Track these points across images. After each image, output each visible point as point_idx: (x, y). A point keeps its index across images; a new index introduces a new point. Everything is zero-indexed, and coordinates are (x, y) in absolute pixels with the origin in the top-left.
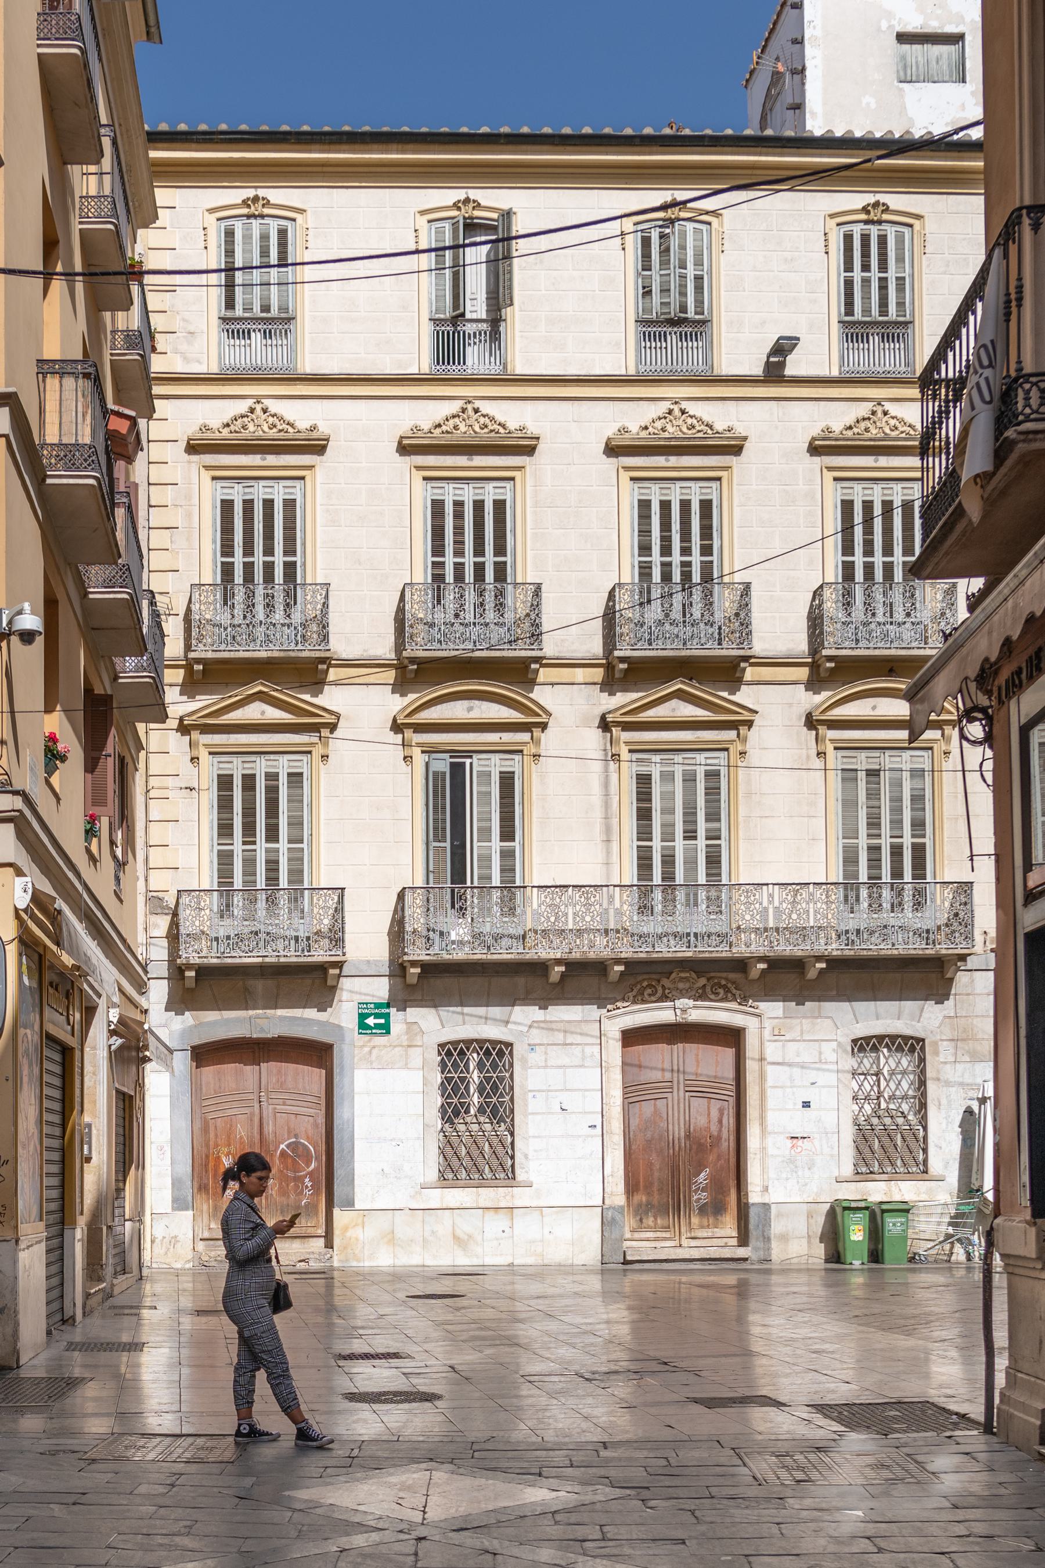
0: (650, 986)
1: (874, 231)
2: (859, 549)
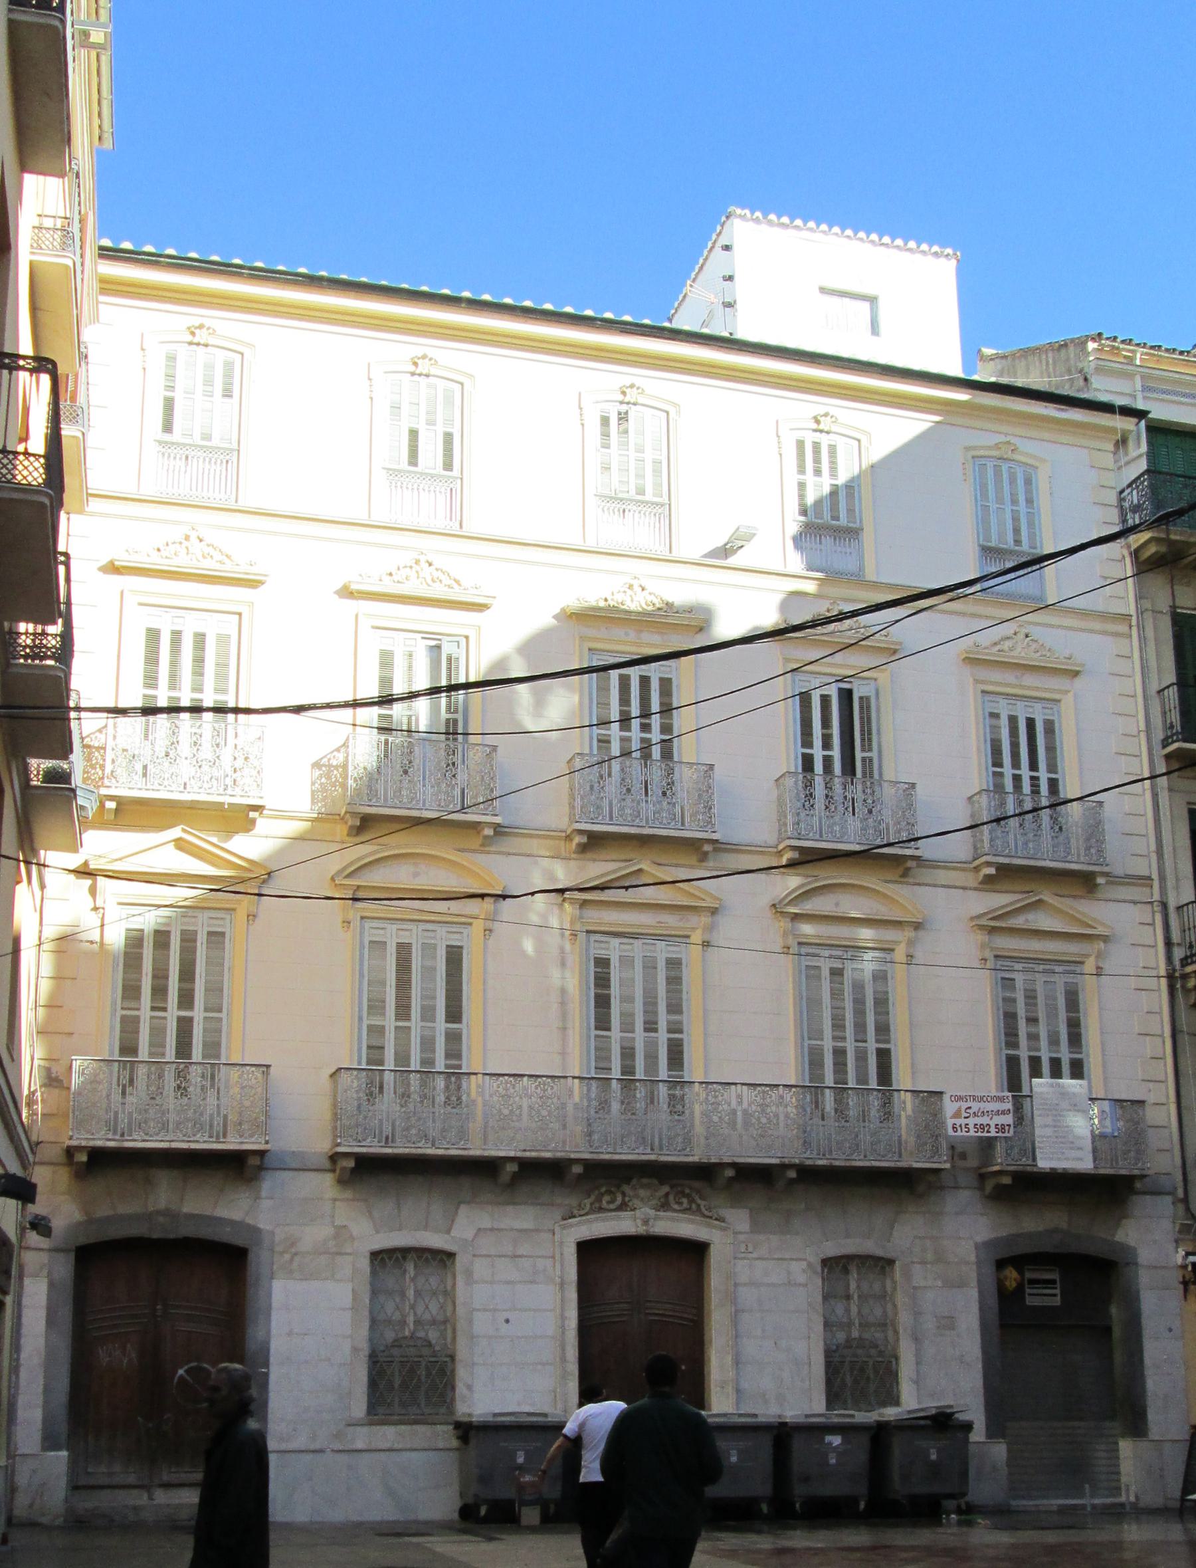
0: (609, 1192)
1: (825, 440)
2: (818, 742)
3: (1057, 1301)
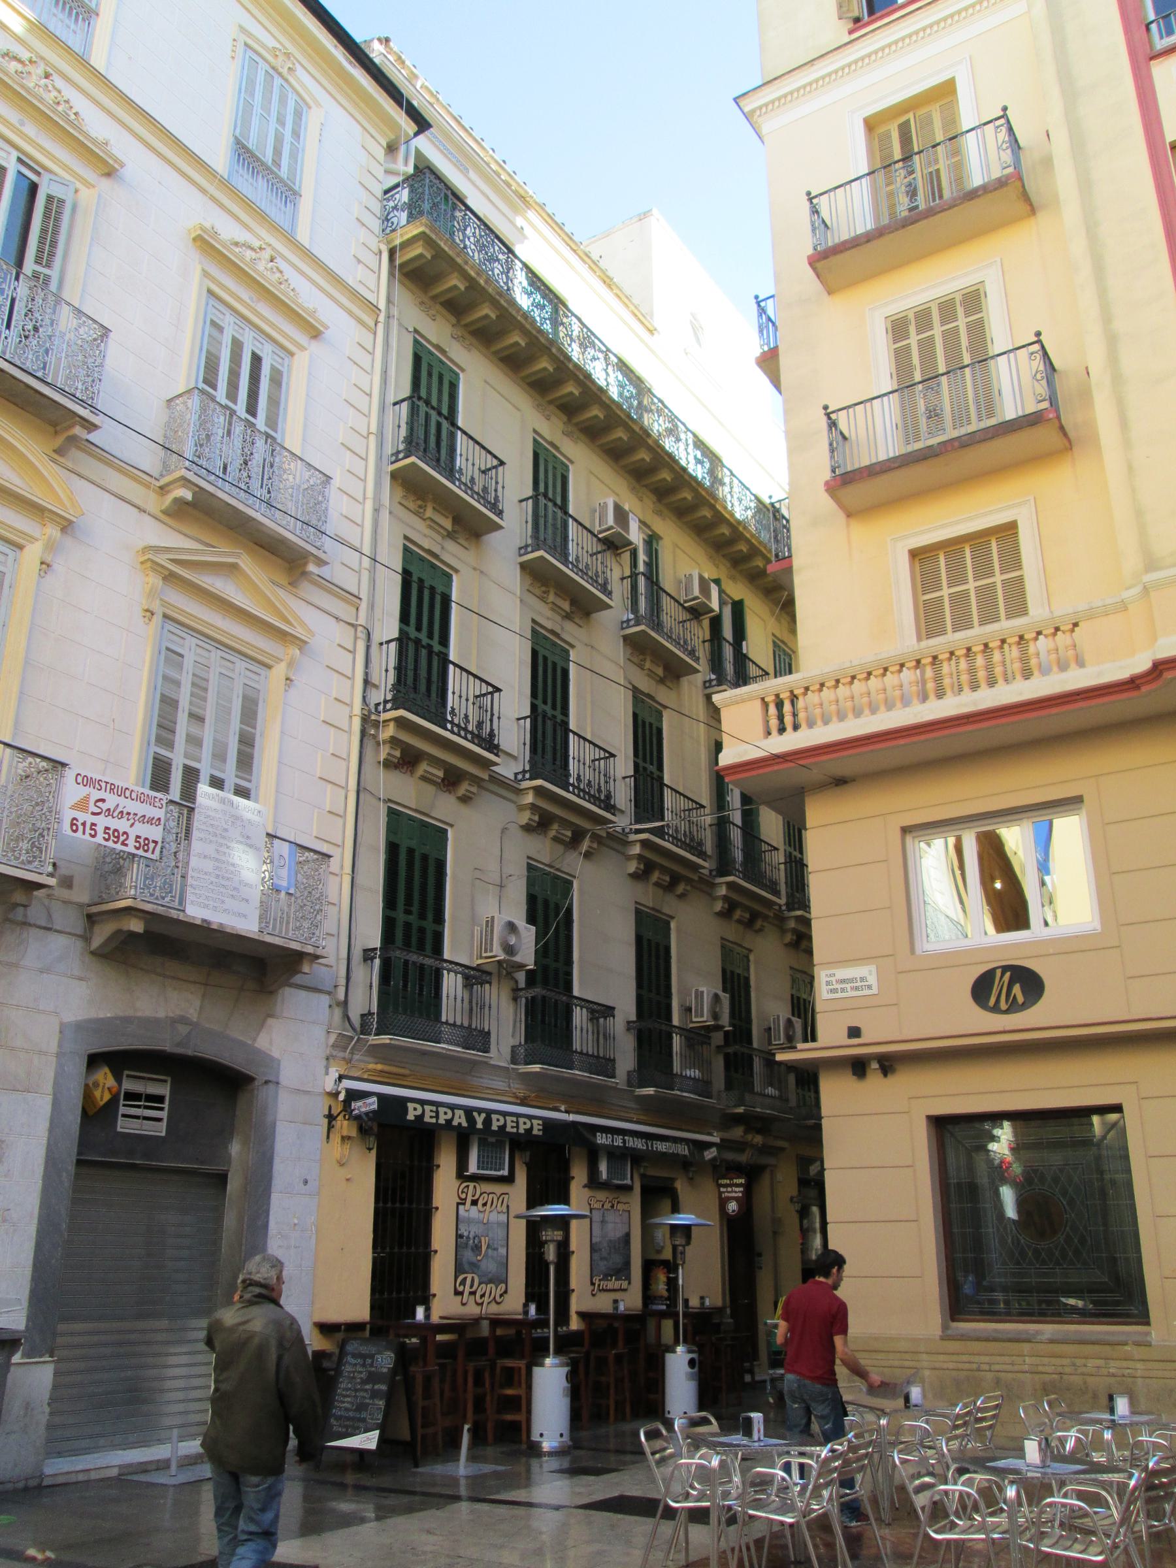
3: (161, 1130)
